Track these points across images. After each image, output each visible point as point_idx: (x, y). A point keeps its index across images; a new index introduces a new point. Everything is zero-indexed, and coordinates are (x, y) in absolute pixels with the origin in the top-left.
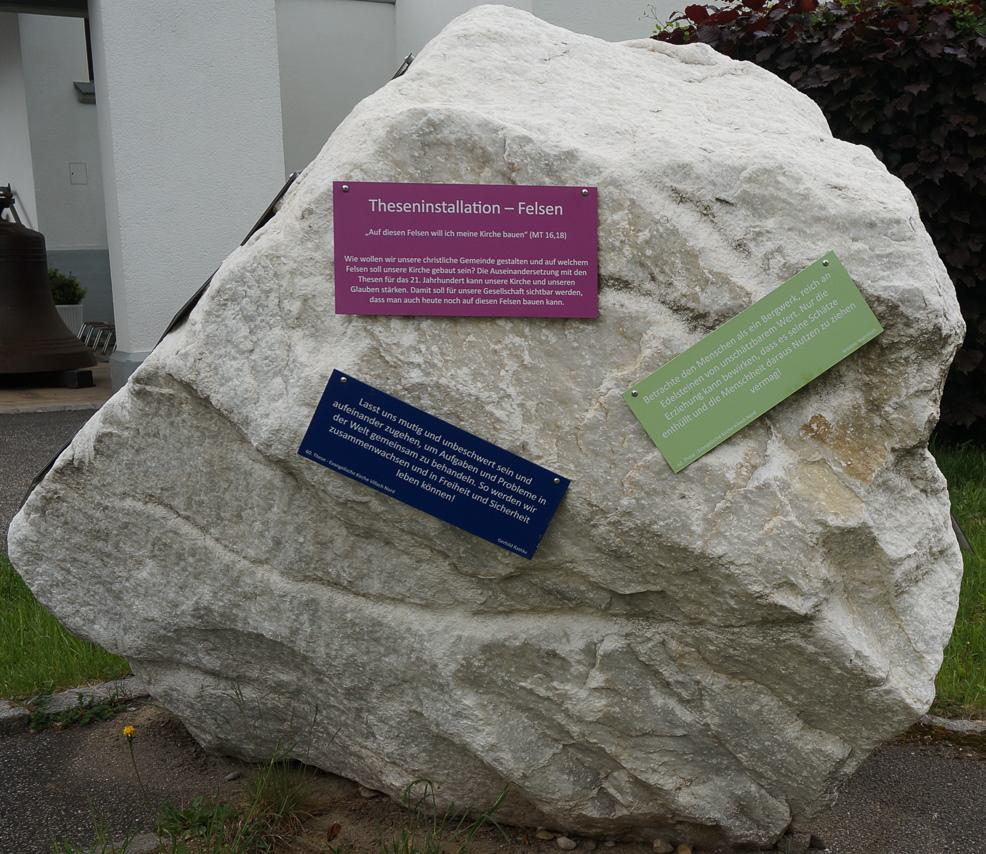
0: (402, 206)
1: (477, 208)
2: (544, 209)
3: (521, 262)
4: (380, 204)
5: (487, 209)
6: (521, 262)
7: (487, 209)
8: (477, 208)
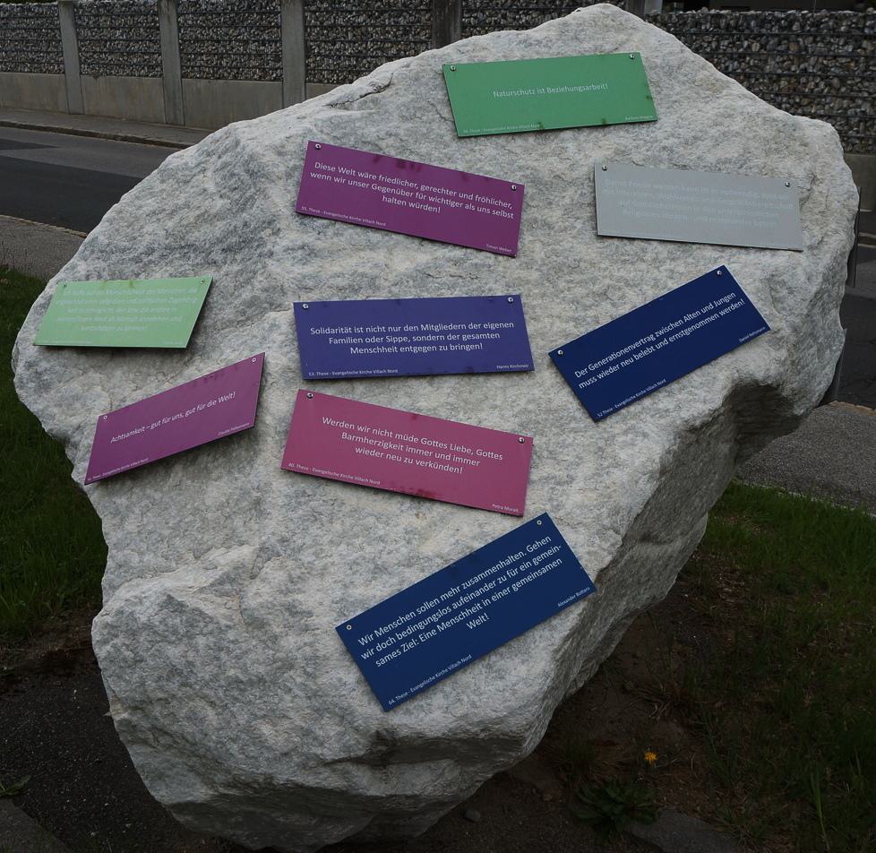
3: (694, 315)
6: (694, 315)
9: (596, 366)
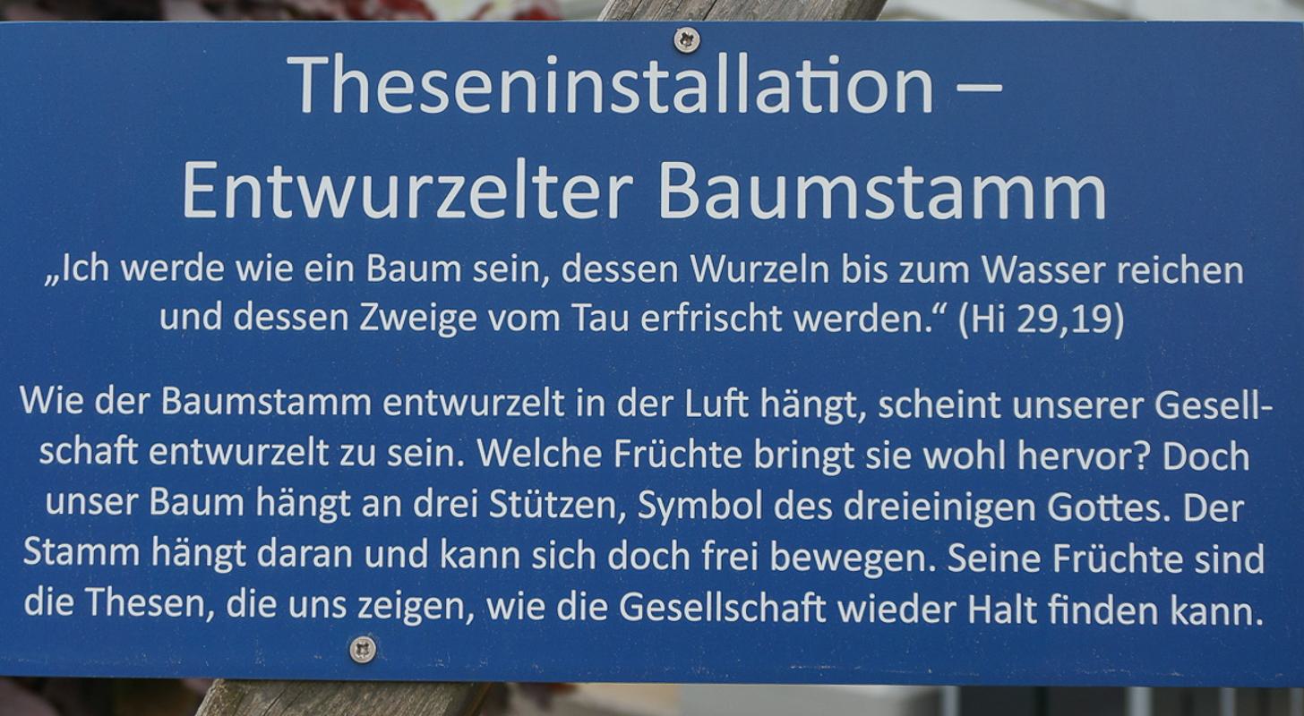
0: (1217, 406)
1: (820, 88)
2: (102, 501)
4: (110, 599)
5: (867, 91)
7: (867, 91)
8: (820, 88)
9: (1188, 408)
